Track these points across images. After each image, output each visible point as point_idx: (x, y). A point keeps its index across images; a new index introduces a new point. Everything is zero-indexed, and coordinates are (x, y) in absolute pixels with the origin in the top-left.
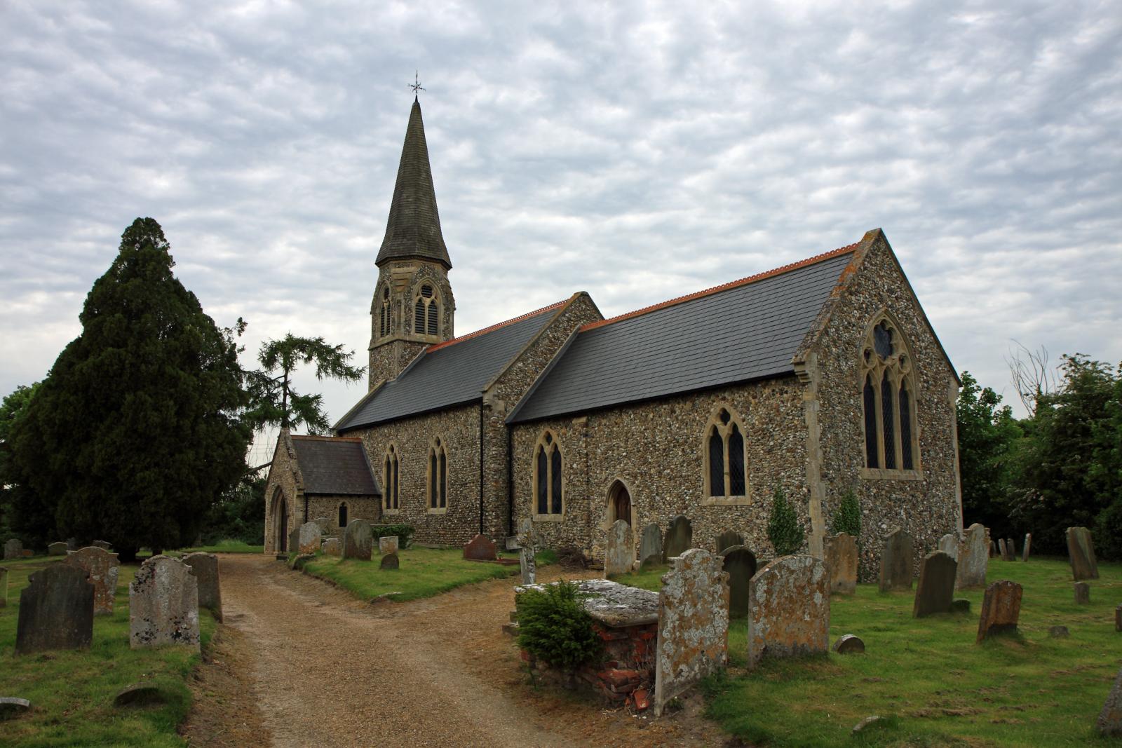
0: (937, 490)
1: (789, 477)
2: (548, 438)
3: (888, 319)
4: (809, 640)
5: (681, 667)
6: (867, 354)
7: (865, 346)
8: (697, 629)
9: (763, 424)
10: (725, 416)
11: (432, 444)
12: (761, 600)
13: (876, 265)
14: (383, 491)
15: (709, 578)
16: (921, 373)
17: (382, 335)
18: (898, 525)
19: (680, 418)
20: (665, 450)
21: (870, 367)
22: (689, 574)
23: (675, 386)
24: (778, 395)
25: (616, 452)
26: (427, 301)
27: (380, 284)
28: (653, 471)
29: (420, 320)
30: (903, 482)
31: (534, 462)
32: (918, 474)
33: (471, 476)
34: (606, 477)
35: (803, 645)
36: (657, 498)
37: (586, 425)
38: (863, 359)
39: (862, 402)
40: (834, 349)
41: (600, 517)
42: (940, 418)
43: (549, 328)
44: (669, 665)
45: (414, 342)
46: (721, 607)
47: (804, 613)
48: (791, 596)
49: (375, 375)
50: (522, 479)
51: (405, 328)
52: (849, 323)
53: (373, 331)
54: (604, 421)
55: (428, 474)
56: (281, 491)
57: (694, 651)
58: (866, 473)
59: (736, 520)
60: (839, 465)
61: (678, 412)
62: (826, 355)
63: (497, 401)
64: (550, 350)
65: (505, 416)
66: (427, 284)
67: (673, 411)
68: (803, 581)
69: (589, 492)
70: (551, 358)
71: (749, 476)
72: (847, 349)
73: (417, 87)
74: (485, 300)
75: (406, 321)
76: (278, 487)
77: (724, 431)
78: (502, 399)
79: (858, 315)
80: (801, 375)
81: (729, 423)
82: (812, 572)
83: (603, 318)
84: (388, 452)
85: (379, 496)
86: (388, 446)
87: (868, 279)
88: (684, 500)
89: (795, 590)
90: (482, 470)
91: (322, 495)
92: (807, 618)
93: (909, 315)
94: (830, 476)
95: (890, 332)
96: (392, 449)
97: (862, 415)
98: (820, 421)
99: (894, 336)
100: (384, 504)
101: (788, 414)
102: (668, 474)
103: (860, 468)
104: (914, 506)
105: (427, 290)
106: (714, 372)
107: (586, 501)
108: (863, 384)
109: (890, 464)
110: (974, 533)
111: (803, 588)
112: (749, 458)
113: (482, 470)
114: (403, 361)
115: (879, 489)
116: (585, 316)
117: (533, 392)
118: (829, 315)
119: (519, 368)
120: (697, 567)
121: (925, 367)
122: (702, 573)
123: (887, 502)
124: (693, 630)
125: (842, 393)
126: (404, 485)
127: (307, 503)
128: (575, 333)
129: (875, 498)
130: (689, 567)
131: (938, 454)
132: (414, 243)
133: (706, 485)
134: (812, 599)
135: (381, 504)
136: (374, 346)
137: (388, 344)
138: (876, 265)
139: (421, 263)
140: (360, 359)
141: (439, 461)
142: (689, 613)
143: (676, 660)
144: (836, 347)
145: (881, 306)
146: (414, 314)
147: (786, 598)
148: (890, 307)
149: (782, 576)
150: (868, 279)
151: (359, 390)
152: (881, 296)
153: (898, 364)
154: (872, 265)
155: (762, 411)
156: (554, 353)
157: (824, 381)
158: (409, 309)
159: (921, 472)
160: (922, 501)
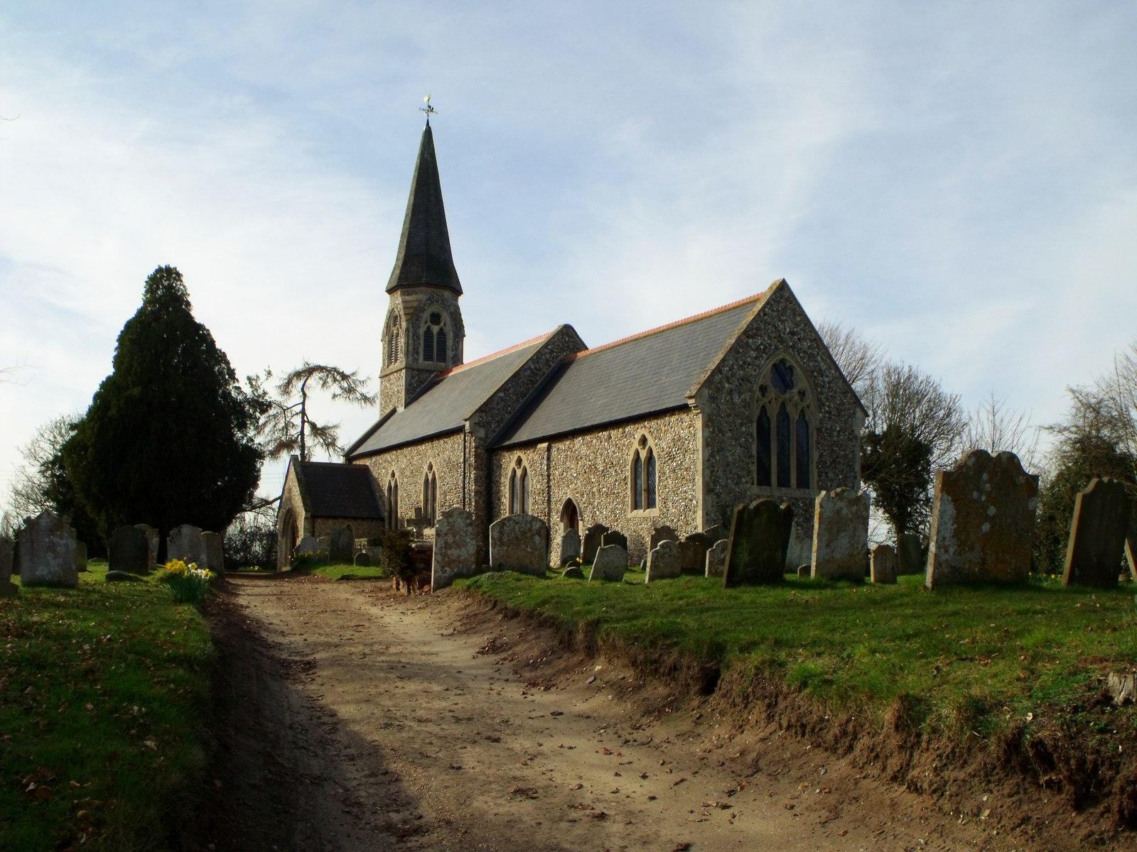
2: (519, 461)
3: (788, 358)
6: (763, 389)
7: (761, 381)
10: (644, 441)
11: (426, 467)
14: (386, 514)
25: (569, 473)
26: (435, 329)
30: (796, 499)
34: (561, 495)
38: (758, 393)
40: (727, 385)
41: (557, 531)
45: (423, 370)
47: (527, 547)
51: (413, 356)
52: (744, 363)
55: (422, 497)
56: (291, 515)
57: (454, 561)
62: (719, 390)
64: (531, 381)
65: (485, 442)
70: (532, 388)
72: (740, 384)
74: (495, 332)
75: (414, 349)
81: (647, 448)
84: (389, 477)
85: (382, 520)
86: (390, 472)
91: (328, 517)
92: (529, 550)
94: (717, 491)
96: (393, 475)
99: (795, 372)
103: (749, 485)
105: (436, 318)
108: (757, 413)
109: (784, 482)
111: (526, 533)
116: (568, 347)
125: (734, 421)
131: (837, 475)
132: (426, 267)
133: (629, 500)
136: (385, 373)
137: (396, 372)
140: (373, 387)
141: (430, 485)
142: (450, 539)
144: (729, 383)
146: (422, 342)
151: (372, 415)
153: (797, 398)
154: (773, 311)
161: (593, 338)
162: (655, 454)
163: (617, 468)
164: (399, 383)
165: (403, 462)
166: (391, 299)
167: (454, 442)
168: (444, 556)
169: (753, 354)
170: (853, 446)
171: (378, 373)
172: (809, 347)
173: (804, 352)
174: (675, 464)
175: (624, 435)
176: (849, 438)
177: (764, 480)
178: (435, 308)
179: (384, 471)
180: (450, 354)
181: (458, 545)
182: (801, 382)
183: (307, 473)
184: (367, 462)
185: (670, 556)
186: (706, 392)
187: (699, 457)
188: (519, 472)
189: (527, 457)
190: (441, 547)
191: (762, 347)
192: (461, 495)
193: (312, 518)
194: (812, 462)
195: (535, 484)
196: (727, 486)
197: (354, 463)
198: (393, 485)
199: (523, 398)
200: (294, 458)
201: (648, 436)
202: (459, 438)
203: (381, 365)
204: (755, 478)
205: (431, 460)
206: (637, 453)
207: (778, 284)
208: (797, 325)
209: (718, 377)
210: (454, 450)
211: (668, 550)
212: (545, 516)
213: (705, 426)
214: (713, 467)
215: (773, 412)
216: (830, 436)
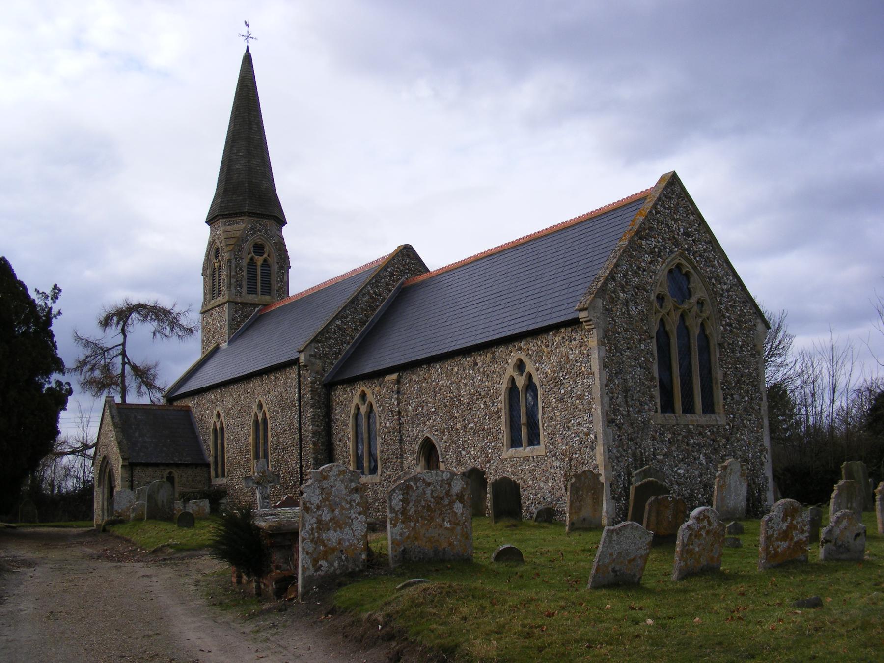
0: (742, 434)
1: (579, 424)
2: (363, 396)
3: (684, 262)
4: (450, 544)
5: (320, 563)
6: (661, 298)
8: (336, 531)
9: (555, 373)
10: (520, 366)
11: (255, 407)
12: (397, 509)
13: (670, 208)
14: (211, 459)
15: (346, 488)
16: (724, 316)
17: (213, 297)
18: (696, 470)
19: (481, 370)
20: (468, 403)
21: (663, 312)
22: (325, 484)
23: (478, 337)
24: (567, 343)
25: (425, 408)
26: (259, 260)
27: (211, 243)
28: (458, 426)
29: (252, 279)
30: (702, 427)
31: (351, 423)
32: (720, 419)
33: (290, 440)
34: (416, 433)
35: (444, 549)
36: (463, 453)
37: (398, 381)
38: (656, 304)
39: (653, 346)
40: (622, 295)
42: (745, 361)
43: (369, 283)
44: (309, 561)
45: (246, 304)
46: (360, 514)
47: (444, 520)
48: (429, 506)
49: (208, 339)
50: (340, 441)
52: (639, 268)
53: (205, 294)
54: (414, 377)
55: (251, 440)
57: (333, 550)
58: (658, 419)
59: (534, 471)
60: (628, 411)
61: (480, 364)
62: (612, 301)
63: (314, 361)
64: (370, 306)
66: (259, 241)
67: (476, 364)
68: (440, 491)
69: (402, 451)
71: (543, 426)
72: (636, 294)
73: (248, 37)
74: (323, 250)
76: (105, 457)
77: (520, 382)
78: (320, 358)
79: (649, 259)
80: (586, 322)
82: (450, 485)
83: (427, 270)
84: (214, 419)
85: (208, 465)
86: (215, 412)
87: (660, 223)
88: (487, 454)
89: (433, 500)
90: (300, 432)
91: (147, 465)
92: (447, 525)
93: (709, 258)
95: (687, 275)
96: (218, 415)
97: (654, 359)
98: (605, 367)
99: (692, 279)
100: (213, 473)
101: (576, 361)
102: (472, 428)
104: (715, 451)
105: (259, 249)
106: (512, 322)
107: (399, 460)
108: (656, 328)
109: (689, 408)
110: (729, 468)
112: (543, 408)
113: (300, 432)
114: (233, 324)
115: (674, 433)
116: (409, 269)
117: (352, 350)
118: (615, 261)
119: (338, 326)
120: (334, 478)
121: (727, 310)
122: (338, 484)
123: (684, 447)
124: (331, 532)
125: (632, 338)
126: (231, 451)
127: (132, 473)
128: (398, 288)
129: (670, 443)
130: (325, 478)
131: (743, 397)
132: (247, 195)
133: (505, 437)
134: (452, 508)
135: (209, 473)
136: (206, 309)
137: (218, 306)
138: (670, 208)
139: (252, 220)
140: (193, 318)
141: (261, 426)
142: (326, 516)
143: (315, 556)
144: (624, 292)
145: (676, 249)
146: (245, 273)
147: (424, 507)
148: (687, 250)
149: (417, 487)
150: (660, 223)
151: (192, 350)
152: (676, 239)
153: (696, 309)
155: (554, 359)
156: (375, 310)
157: (610, 327)
158: (240, 269)
159: (723, 417)
160: (725, 445)
161: (434, 259)
162: (536, 380)
163: (488, 400)
164: (222, 318)
165: (229, 402)
166: (211, 230)
167: (286, 378)
168: (316, 543)
169: (648, 258)
170: (757, 362)
171: (198, 306)
172: (705, 250)
173: (700, 256)
174: (563, 392)
175: (494, 360)
176: (752, 354)
177: (667, 406)
178: (258, 238)
179: (208, 413)
180: (275, 287)
181: (338, 525)
182: (700, 293)
183: (122, 417)
184: (190, 403)
185: (708, 532)
186: (600, 303)
187: (597, 382)
188: (363, 409)
189: (372, 391)
190: (312, 529)
191: (656, 250)
192: (297, 436)
193: (130, 466)
194: (717, 383)
195: (383, 423)
196: (628, 415)
197: (175, 404)
198: (260, 419)
199: (362, 326)
200: (109, 403)
201: (526, 360)
202: (293, 373)
203: (202, 300)
204: (659, 404)
205: (260, 398)
206: (513, 380)
207: (667, 178)
208: (691, 225)
209: (611, 285)
210: (287, 386)
211: (705, 523)
212: (397, 458)
213: (601, 343)
214: (612, 393)
215: (672, 326)
216: (733, 351)
